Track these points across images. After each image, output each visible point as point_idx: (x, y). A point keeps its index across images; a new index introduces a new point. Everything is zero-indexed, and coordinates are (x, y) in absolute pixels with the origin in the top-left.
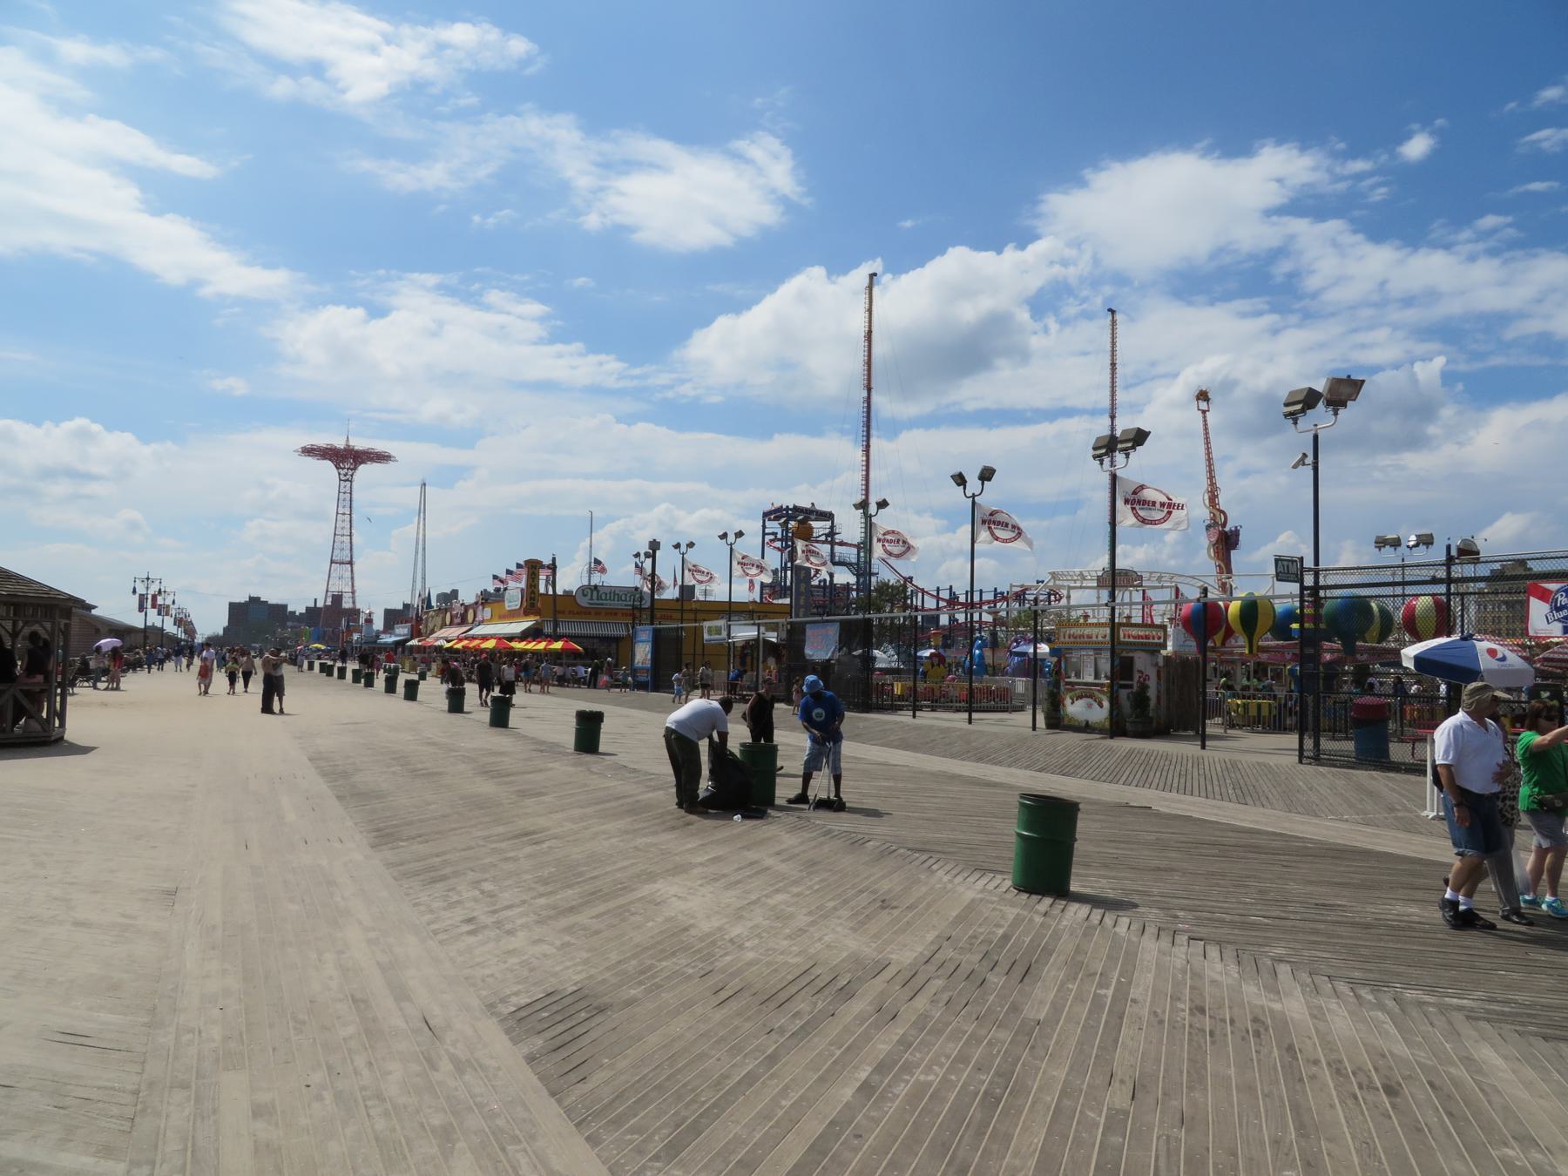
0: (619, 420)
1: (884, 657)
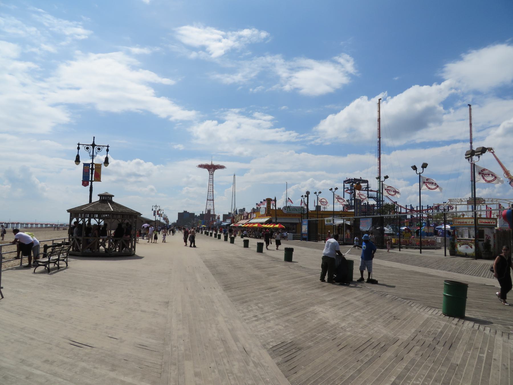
0: (296, 152)
1: (388, 230)
